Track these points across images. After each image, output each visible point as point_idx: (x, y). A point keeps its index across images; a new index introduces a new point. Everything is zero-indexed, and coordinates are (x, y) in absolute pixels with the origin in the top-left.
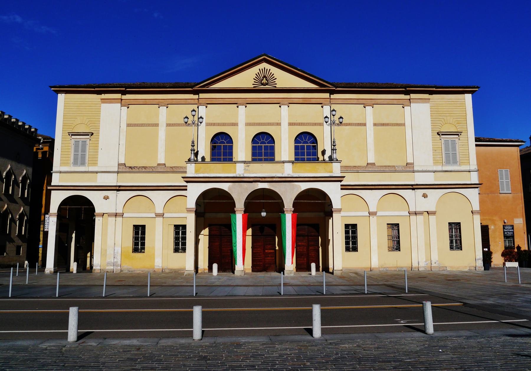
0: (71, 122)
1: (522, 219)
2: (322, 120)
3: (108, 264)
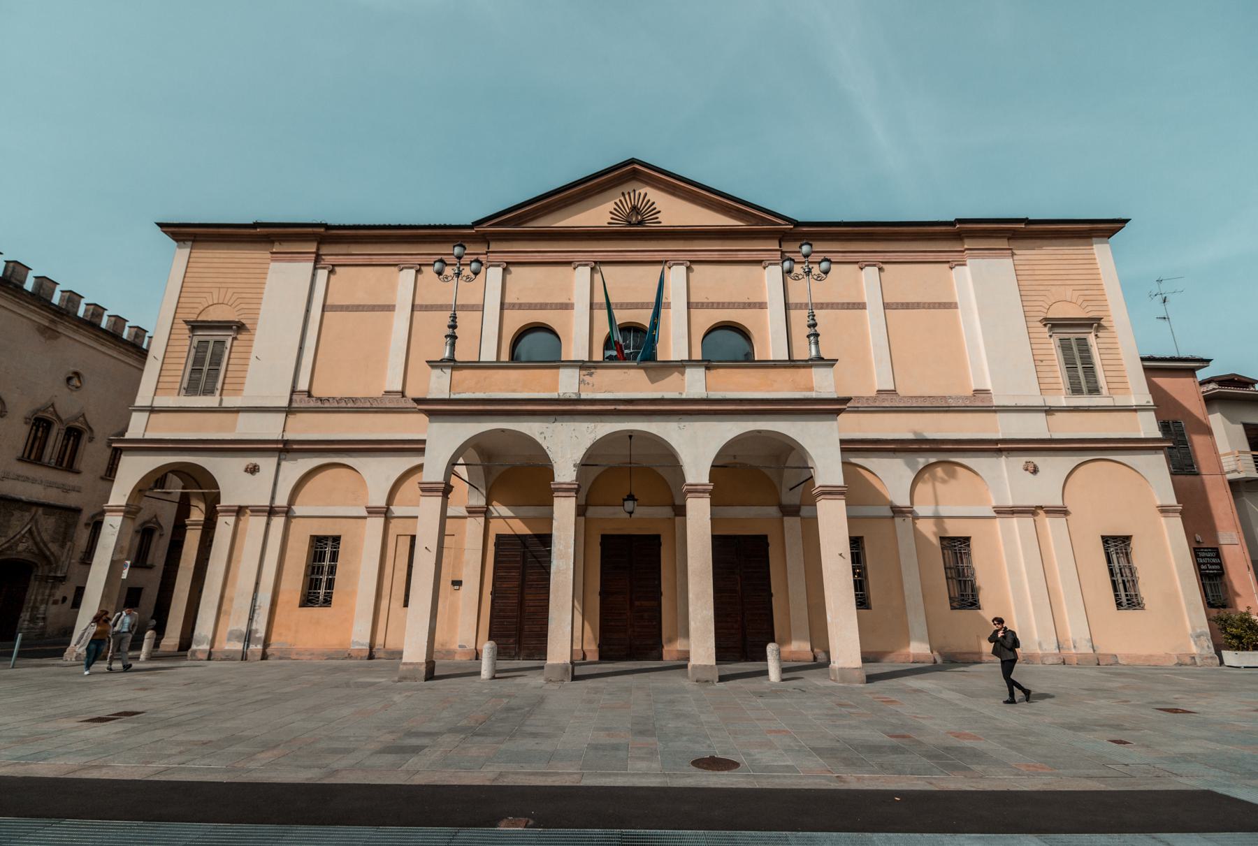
0: (198, 300)
1: (1234, 534)
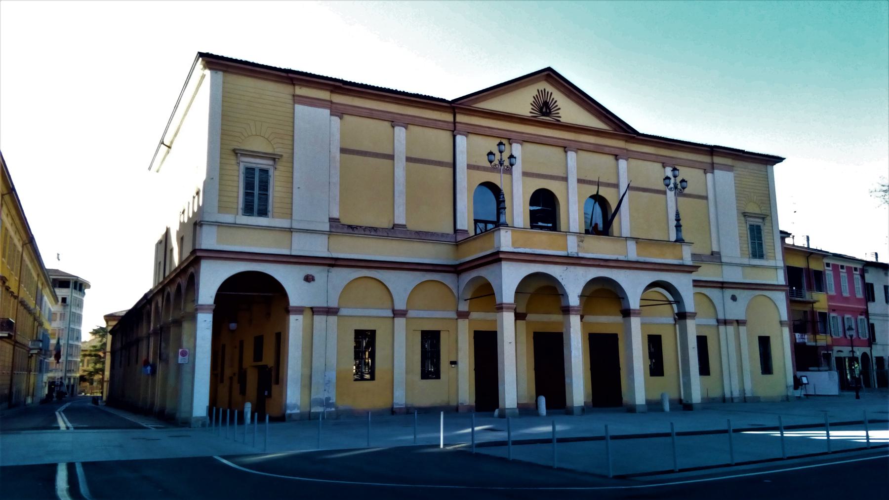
2: (662, 187)
3: (321, 403)
